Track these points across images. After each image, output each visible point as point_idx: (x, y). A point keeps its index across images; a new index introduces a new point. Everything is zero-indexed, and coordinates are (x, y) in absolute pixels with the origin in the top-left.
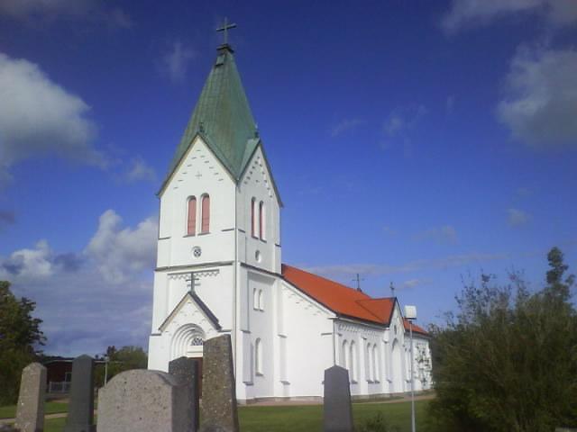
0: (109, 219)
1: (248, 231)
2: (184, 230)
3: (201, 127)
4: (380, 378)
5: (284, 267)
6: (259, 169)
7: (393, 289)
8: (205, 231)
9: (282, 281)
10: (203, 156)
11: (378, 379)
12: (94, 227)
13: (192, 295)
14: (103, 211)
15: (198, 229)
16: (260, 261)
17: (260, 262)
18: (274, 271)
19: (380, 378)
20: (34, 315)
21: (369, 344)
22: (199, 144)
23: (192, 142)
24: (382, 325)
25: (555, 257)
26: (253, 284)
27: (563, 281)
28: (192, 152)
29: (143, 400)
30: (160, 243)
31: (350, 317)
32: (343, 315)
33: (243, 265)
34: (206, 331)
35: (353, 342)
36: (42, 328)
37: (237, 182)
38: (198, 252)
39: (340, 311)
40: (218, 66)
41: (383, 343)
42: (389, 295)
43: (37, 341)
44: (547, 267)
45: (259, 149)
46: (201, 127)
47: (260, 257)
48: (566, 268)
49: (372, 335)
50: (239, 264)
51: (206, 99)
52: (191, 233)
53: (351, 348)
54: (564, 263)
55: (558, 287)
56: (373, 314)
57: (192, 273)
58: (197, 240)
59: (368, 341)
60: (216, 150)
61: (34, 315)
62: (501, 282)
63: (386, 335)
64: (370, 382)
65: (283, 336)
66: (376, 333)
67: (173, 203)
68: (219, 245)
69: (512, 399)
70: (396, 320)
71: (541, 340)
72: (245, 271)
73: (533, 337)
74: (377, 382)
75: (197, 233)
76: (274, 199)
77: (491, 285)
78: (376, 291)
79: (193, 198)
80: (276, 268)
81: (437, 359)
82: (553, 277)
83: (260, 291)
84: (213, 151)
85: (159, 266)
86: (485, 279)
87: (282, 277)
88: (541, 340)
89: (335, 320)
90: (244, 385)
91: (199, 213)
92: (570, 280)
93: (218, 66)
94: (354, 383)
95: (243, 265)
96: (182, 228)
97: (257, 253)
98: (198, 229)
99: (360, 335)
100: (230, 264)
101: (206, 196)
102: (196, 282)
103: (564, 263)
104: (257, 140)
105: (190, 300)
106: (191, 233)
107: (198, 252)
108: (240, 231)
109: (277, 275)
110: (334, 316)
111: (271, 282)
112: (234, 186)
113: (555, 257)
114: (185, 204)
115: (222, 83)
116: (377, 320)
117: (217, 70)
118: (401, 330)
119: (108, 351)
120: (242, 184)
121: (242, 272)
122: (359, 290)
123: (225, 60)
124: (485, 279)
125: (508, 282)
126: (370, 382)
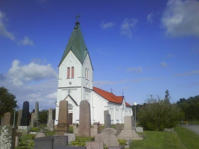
0: (15, 63)
1: (84, 78)
4: (119, 119)
5: (94, 87)
7: (123, 93)
8: (73, 77)
9: (93, 92)
10: (72, 56)
11: (113, 119)
12: (11, 66)
13: (69, 95)
14: (14, 59)
15: (71, 77)
16: (87, 86)
17: (87, 86)
18: (91, 89)
19: (119, 119)
20: (15, 100)
21: (111, 109)
22: (71, 52)
23: (69, 51)
24: (120, 104)
25: (167, 92)
31: (112, 102)
32: (110, 102)
33: (84, 87)
34: (73, 106)
35: (112, 109)
36: (17, 103)
37: (82, 64)
38: (70, 83)
39: (110, 100)
40: (75, 28)
41: (120, 109)
43: (16, 108)
45: (88, 54)
47: (88, 85)
48: (169, 95)
49: (117, 107)
50: (83, 87)
51: (72, 39)
52: (68, 78)
53: (112, 111)
54: (169, 93)
55: (167, 99)
56: (117, 100)
57: (69, 89)
59: (110, 108)
60: (75, 54)
61: (15, 100)
62: (155, 97)
63: (121, 107)
64: (117, 120)
65: (93, 107)
66: (118, 106)
68: (77, 81)
69: (156, 123)
70: (124, 103)
71: (162, 111)
72: (84, 89)
73: (161, 110)
74: (118, 120)
75: (70, 78)
77: (153, 97)
78: (117, 94)
79: (69, 68)
80: (91, 88)
82: (166, 96)
83: (88, 95)
84: (75, 55)
85: (59, 87)
86: (151, 96)
87: (93, 91)
88: (162, 111)
89: (108, 103)
90: (116, 121)
91: (71, 72)
92: (170, 97)
94: (112, 120)
95: (84, 87)
97: (87, 84)
98: (71, 77)
99: (114, 107)
100: (80, 87)
101: (73, 67)
102: (70, 92)
103: (169, 93)
104: (87, 52)
105: (69, 97)
107: (70, 83)
108: (83, 78)
109: (92, 90)
110: (108, 102)
111: (90, 92)
112: (81, 65)
113: (167, 92)
116: (119, 103)
117: (75, 30)
118: (125, 105)
119: (33, 111)
120: (83, 64)
121: (83, 89)
122: (112, 93)
123: (78, 26)
124: (151, 96)
125: (157, 97)
126: (117, 120)
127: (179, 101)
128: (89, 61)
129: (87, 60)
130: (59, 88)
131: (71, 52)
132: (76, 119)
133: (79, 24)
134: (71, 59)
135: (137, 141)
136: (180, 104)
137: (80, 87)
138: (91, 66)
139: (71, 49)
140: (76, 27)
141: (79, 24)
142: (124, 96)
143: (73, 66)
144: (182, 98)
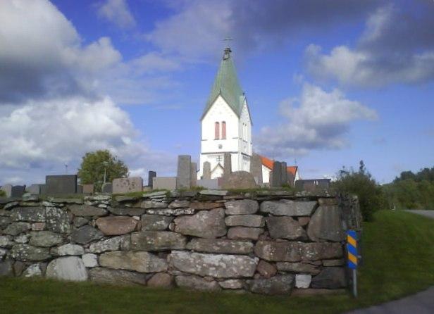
2: (214, 137)
6: (245, 112)
8: (224, 137)
15: (221, 137)
17: (245, 152)
22: (220, 98)
23: (217, 97)
25: (362, 163)
27: (363, 169)
28: (217, 102)
30: (203, 142)
33: (242, 154)
37: (239, 117)
38: (220, 147)
40: (225, 59)
44: (360, 166)
45: (212, 169)
52: (217, 138)
58: (220, 142)
67: (208, 126)
76: (250, 123)
79: (217, 123)
82: (361, 168)
85: (203, 151)
86: (344, 167)
93: (225, 59)
95: (242, 154)
98: (221, 137)
100: (236, 153)
101: (224, 122)
105: (219, 168)
107: (220, 147)
112: (237, 119)
113: (362, 163)
114: (213, 127)
115: (268, 186)
127: (399, 176)
128: (217, 105)
129: (245, 112)
130: (203, 154)
131: (220, 98)
132: (105, 206)
133: (230, 51)
134: (220, 110)
135: (351, 236)
136: (401, 182)
137: (236, 153)
138: (249, 120)
139: (220, 94)
140: (226, 56)
141: (230, 51)
142: (297, 167)
143: (225, 120)
144: (407, 170)
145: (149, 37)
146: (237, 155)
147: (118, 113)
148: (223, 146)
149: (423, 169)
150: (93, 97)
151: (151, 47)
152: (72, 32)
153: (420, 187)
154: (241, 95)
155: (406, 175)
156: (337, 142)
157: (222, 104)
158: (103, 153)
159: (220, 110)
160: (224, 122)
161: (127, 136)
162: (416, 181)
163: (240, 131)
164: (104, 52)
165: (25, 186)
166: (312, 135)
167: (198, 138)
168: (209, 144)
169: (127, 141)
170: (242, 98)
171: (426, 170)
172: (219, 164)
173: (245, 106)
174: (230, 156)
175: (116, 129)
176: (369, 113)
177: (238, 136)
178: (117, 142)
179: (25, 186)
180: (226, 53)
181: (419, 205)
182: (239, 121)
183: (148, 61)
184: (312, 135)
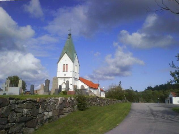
0: (70, 90)
3: (66, 51)
5: (80, 78)
6: (76, 60)
8: (67, 71)
15: (65, 71)
17: (76, 77)
22: (66, 54)
23: (65, 53)
25: (120, 82)
26: (75, 81)
29: (48, 101)
30: (58, 73)
33: (74, 78)
37: (73, 63)
38: (65, 75)
42: (98, 83)
44: (119, 83)
45: (76, 56)
46: (66, 51)
52: (64, 71)
58: (65, 73)
68: (69, 74)
70: (99, 88)
76: (78, 65)
79: (64, 65)
81: (118, 86)
82: (120, 84)
87: (79, 80)
91: (65, 67)
96: (62, 70)
98: (65, 71)
100: (71, 77)
101: (67, 64)
105: (64, 84)
106: (64, 71)
107: (65, 75)
110: (89, 87)
111: (77, 81)
112: (73, 63)
113: (120, 82)
127: (147, 88)
129: (76, 60)
131: (66, 54)
133: (70, 35)
134: (66, 59)
137: (71, 77)
138: (78, 63)
139: (66, 52)
140: (69, 37)
141: (71, 35)
145: (45, 28)
146: (72, 78)
147: (36, 60)
148: (66, 74)
149: (156, 86)
150: (24, 51)
151: (46, 32)
152: (13, 23)
153: (153, 93)
154: (74, 53)
155: (149, 88)
156: (127, 73)
157: (67, 57)
158: (15, 77)
159: (66, 59)
160: (67, 64)
161: (40, 70)
162: (152, 90)
163: (74, 68)
164: (28, 31)
165: (146, 89)
166: (118, 70)
167: (56, 71)
168: (60, 74)
169: (39, 72)
170: (75, 54)
171: (157, 86)
172: (64, 82)
173: (76, 58)
174: (58, 79)
175: (33, 67)
176: (142, 62)
177: (72, 70)
178: (35, 72)
179: (146, 89)
180: (69, 36)
181: (152, 101)
182: (73, 64)
183: (45, 38)
184: (118, 70)
